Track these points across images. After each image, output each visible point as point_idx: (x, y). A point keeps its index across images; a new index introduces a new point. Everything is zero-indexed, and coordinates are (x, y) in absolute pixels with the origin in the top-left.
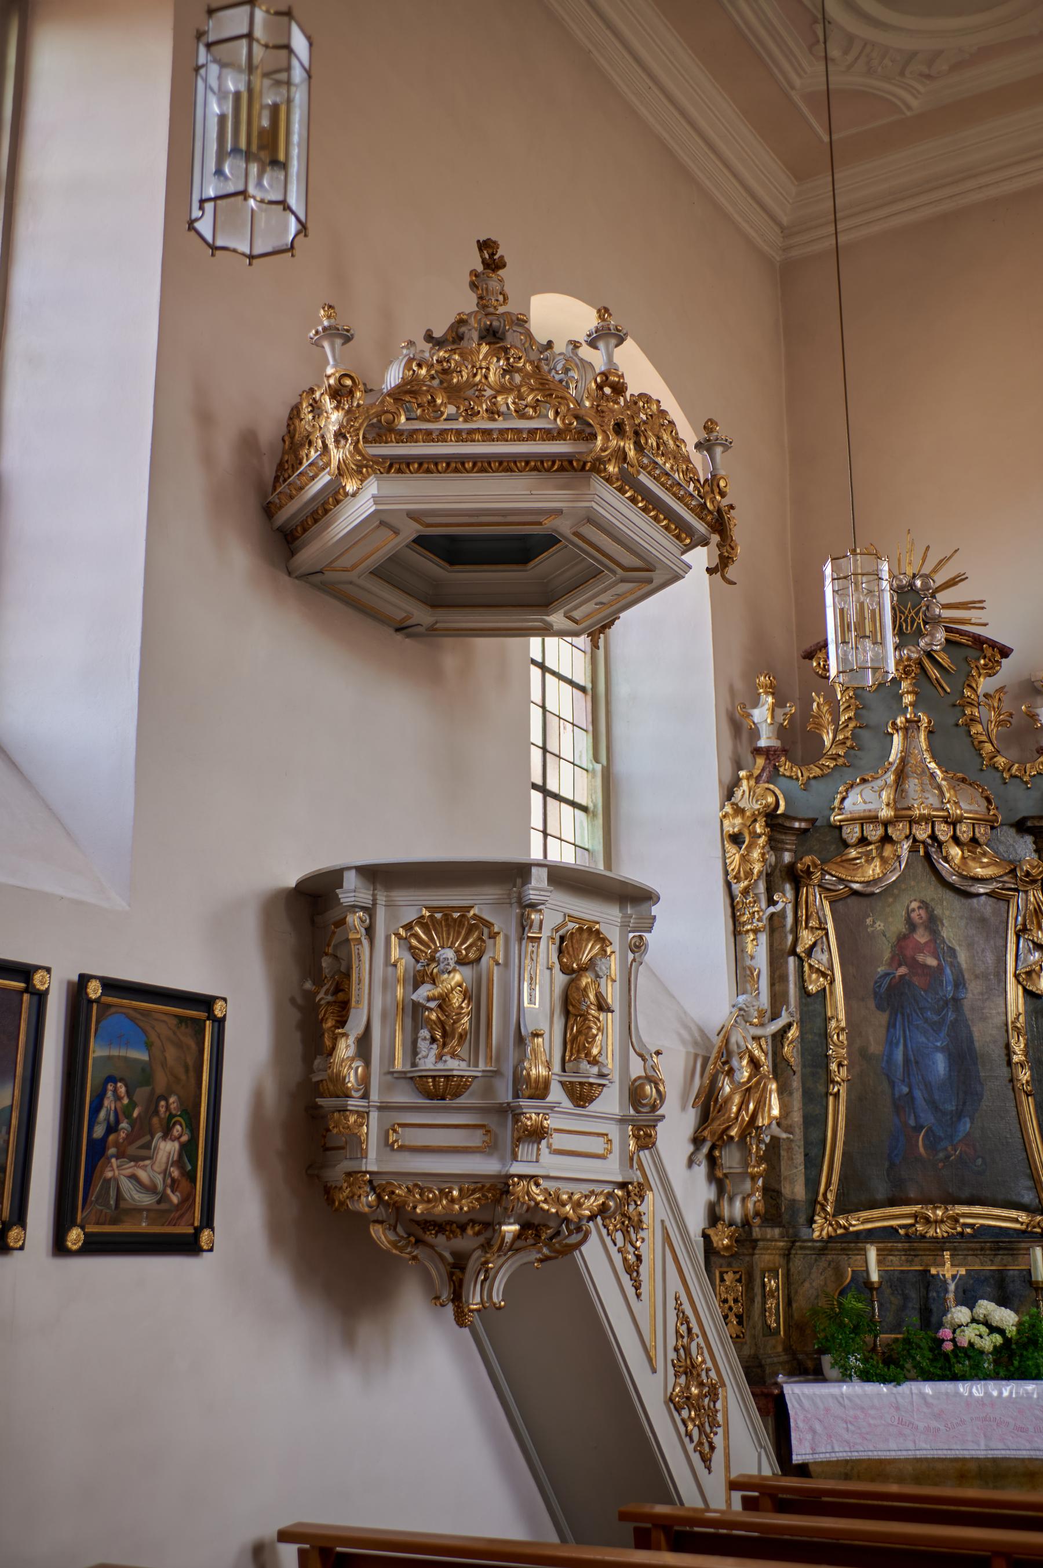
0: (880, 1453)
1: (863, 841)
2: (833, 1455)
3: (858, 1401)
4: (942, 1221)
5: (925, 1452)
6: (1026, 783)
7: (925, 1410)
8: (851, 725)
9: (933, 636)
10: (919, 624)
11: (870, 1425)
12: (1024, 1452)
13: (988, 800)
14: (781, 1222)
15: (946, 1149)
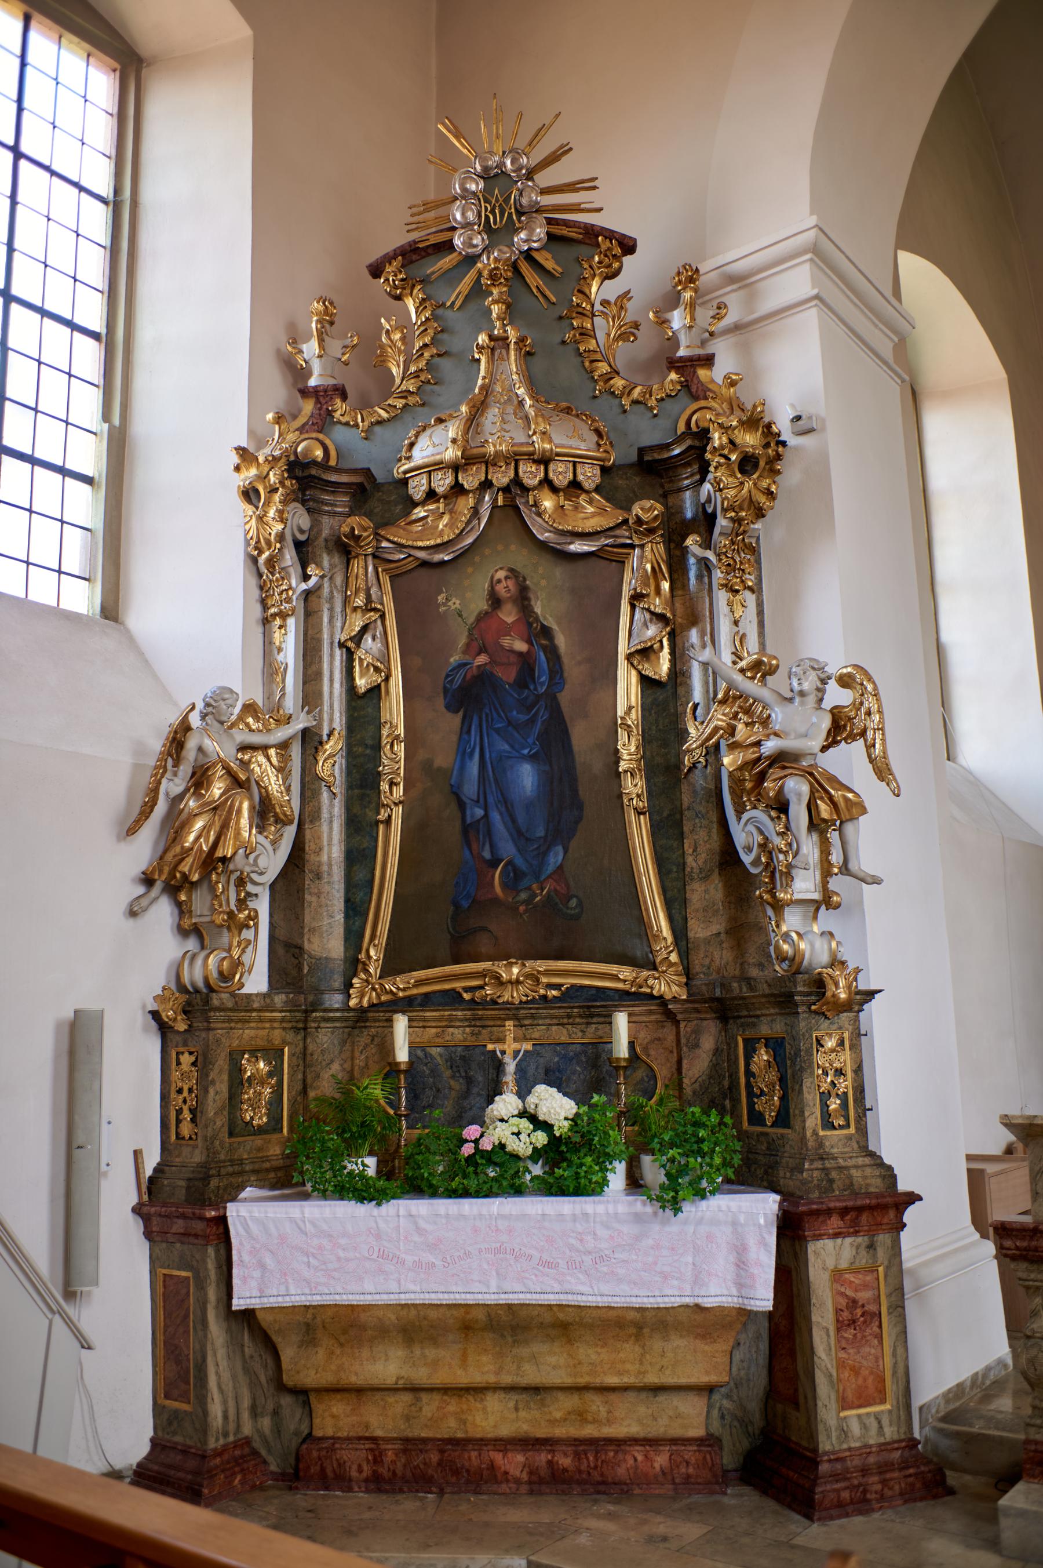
0: (351, 1297)
1: (431, 495)
2: (287, 1299)
3: (325, 1227)
4: (518, 982)
5: (412, 1296)
6: (651, 409)
7: (416, 1238)
8: (427, 355)
9: (532, 231)
10: (510, 214)
11: (339, 1259)
12: (551, 1297)
13: (598, 433)
14: (301, 987)
15: (529, 888)
